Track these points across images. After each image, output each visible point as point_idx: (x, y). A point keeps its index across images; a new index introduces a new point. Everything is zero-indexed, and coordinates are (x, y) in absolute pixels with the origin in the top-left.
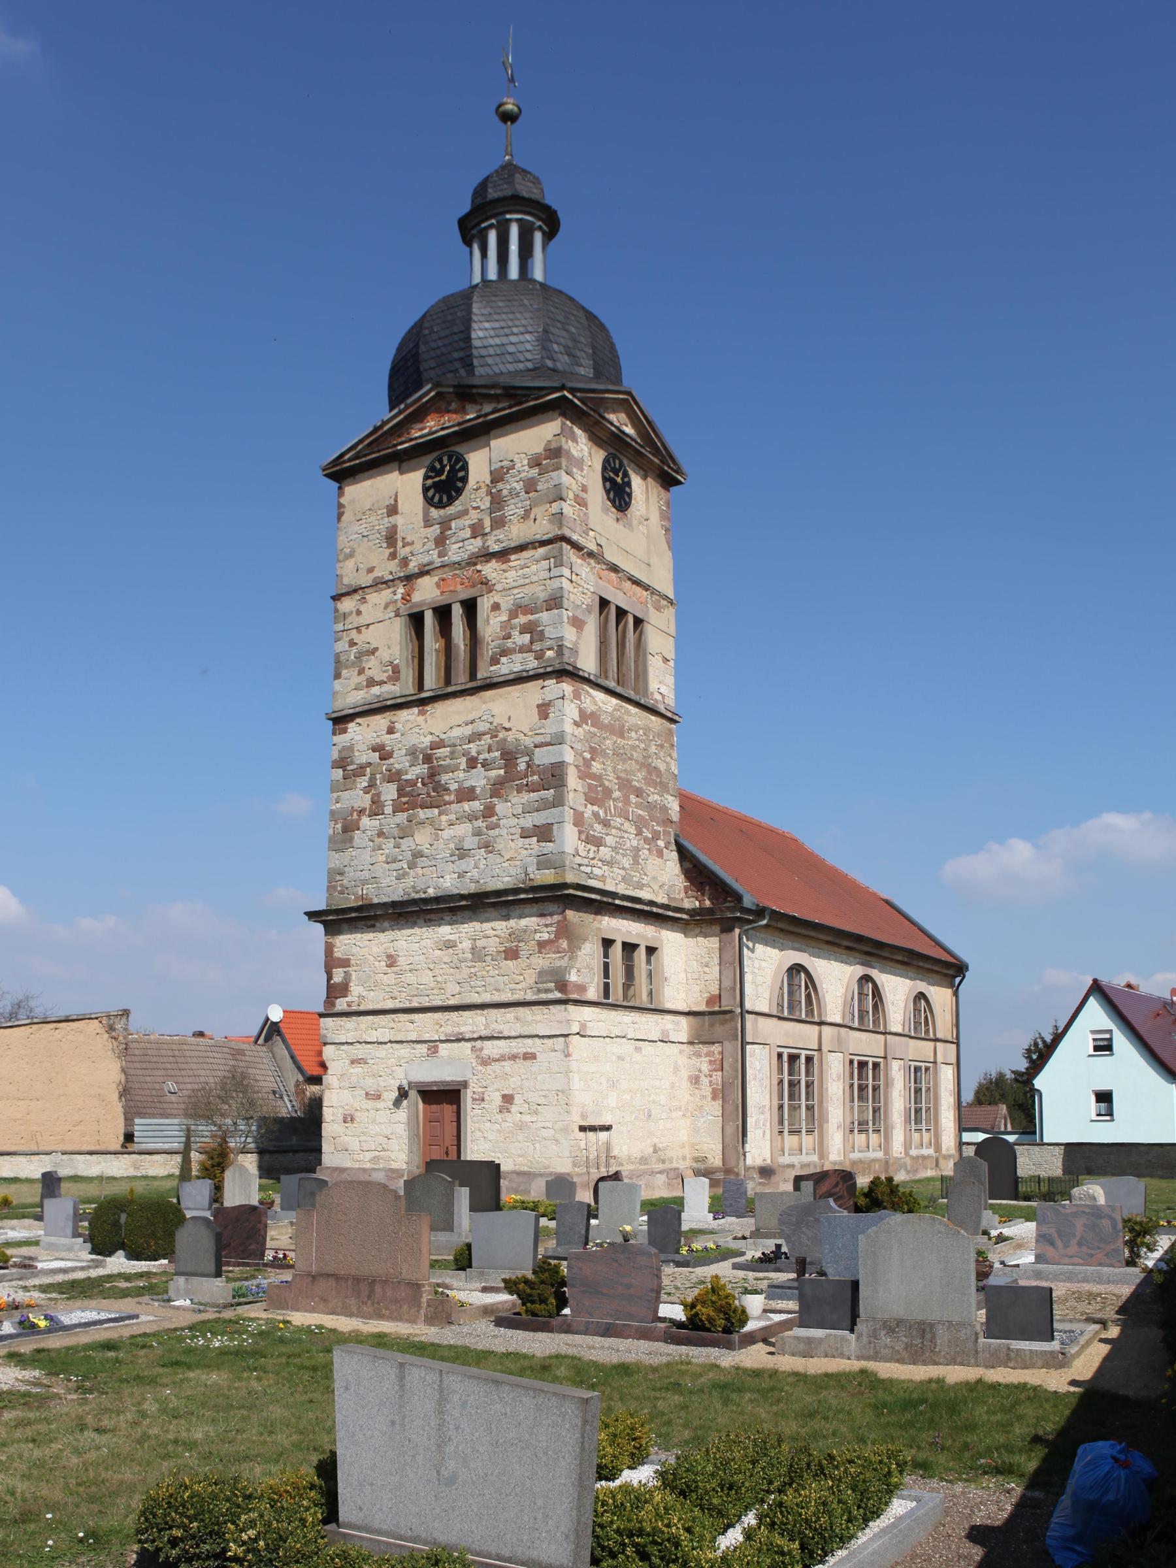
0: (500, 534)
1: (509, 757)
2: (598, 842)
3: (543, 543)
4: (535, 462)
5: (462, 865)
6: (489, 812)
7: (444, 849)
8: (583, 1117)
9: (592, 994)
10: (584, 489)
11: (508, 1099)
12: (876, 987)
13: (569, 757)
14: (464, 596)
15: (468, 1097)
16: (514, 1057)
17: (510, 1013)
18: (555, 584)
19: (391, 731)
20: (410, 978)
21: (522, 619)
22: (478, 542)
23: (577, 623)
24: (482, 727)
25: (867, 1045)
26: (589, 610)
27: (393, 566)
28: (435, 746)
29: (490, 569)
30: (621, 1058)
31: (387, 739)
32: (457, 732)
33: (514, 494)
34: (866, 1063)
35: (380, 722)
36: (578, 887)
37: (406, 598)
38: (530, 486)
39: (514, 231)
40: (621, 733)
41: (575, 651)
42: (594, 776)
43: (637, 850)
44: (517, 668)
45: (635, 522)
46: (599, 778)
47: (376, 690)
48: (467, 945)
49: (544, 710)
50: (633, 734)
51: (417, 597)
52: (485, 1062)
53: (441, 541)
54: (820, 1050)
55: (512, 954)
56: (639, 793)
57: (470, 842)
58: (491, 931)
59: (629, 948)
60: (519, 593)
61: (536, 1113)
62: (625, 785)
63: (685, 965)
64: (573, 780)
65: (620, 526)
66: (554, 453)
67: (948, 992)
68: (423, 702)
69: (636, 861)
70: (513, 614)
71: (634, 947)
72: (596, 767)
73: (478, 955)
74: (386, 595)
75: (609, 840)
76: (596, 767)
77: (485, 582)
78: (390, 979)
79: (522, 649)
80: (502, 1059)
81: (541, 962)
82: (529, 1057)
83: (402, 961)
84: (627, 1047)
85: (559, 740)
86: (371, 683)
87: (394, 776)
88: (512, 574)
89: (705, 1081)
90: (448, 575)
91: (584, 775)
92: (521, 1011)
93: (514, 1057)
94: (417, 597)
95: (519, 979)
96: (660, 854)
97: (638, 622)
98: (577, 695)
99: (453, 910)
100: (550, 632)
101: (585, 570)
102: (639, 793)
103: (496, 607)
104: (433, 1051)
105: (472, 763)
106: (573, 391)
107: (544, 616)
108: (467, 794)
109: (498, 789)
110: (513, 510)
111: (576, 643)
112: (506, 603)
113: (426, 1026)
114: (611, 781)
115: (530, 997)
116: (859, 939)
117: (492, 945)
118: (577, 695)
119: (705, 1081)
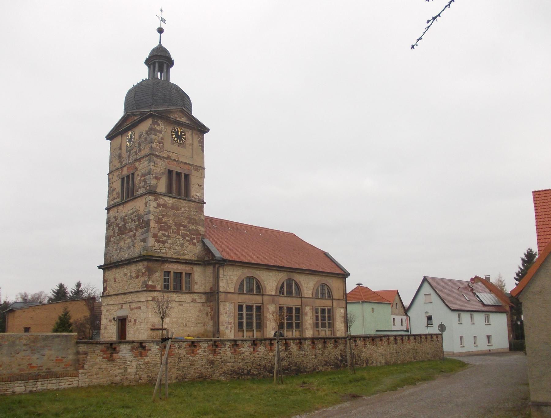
1: (139, 217)
2: (164, 242)
3: (147, 156)
5: (129, 251)
6: (135, 235)
8: (153, 326)
11: (135, 321)
12: (297, 284)
13: (151, 217)
18: (149, 167)
19: (117, 212)
21: (143, 178)
23: (157, 178)
24: (134, 210)
27: (119, 164)
28: (126, 216)
29: (137, 164)
31: (117, 215)
32: (130, 212)
33: (143, 142)
38: (146, 139)
39: (157, 65)
40: (177, 209)
42: (163, 223)
45: (187, 146)
47: (115, 201)
48: (129, 275)
49: (146, 204)
50: (183, 209)
51: (123, 174)
52: (131, 309)
53: (129, 156)
54: (263, 304)
55: (137, 277)
56: (184, 226)
60: (143, 171)
61: (140, 325)
63: (201, 278)
64: (152, 224)
65: (180, 148)
66: (151, 131)
68: (124, 203)
72: (164, 220)
82: (140, 308)
83: (117, 280)
85: (149, 213)
89: (209, 314)
90: (129, 166)
91: (157, 222)
95: (137, 284)
96: (194, 244)
97: (187, 176)
103: (138, 175)
106: (153, 111)
107: (147, 177)
108: (131, 230)
113: (120, 300)
114: (171, 223)
115: (140, 289)
116: (279, 267)
117: (134, 274)
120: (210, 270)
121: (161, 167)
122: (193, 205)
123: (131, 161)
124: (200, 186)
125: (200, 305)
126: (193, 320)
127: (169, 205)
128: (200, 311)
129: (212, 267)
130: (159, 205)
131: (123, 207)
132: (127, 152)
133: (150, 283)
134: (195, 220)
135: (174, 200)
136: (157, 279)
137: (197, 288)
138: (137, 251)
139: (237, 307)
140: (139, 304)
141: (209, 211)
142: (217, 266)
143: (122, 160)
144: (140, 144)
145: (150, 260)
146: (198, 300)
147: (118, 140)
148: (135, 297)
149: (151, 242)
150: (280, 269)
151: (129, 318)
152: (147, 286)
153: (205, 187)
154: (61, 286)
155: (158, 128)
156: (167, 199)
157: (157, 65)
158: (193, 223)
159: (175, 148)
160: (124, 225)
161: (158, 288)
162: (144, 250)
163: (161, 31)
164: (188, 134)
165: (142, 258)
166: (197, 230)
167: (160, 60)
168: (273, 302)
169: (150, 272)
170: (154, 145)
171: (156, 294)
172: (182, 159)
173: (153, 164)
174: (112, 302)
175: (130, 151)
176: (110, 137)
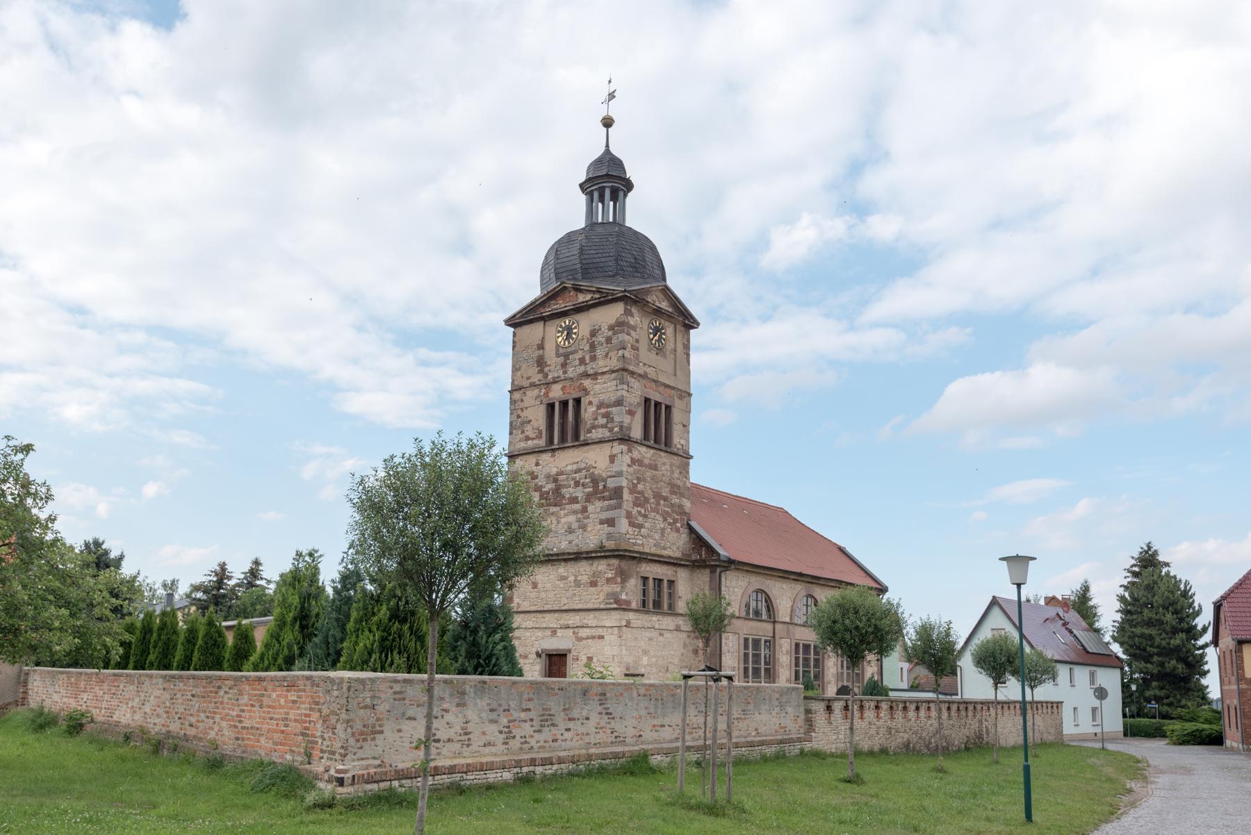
0: (593, 365)
1: (595, 481)
2: (640, 526)
3: (613, 372)
4: (611, 328)
5: (570, 537)
6: (585, 510)
7: (561, 529)
8: (628, 669)
9: (634, 605)
10: (637, 341)
14: (576, 396)
15: (569, 658)
16: (593, 637)
17: (592, 615)
19: (537, 464)
20: (543, 595)
21: (603, 411)
22: (582, 368)
23: (631, 413)
24: (583, 465)
25: (762, 629)
26: (639, 404)
29: (587, 383)
30: (651, 639)
31: (534, 468)
32: (569, 468)
34: (759, 640)
35: (532, 459)
36: (626, 550)
37: (546, 394)
38: (609, 340)
40: (655, 468)
41: (629, 428)
42: (639, 492)
43: (663, 530)
44: (600, 436)
46: (642, 493)
47: (530, 442)
48: (572, 578)
49: (612, 459)
51: (551, 395)
52: (579, 639)
53: (564, 365)
55: (593, 584)
56: (665, 499)
57: (575, 525)
58: (584, 570)
59: (659, 581)
60: (602, 397)
62: (658, 496)
64: (626, 495)
65: (659, 357)
66: (618, 327)
67: (515, 616)
69: (663, 535)
70: (599, 407)
71: (660, 581)
72: (640, 487)
73: (578, 584)
74: (536, 392)
75: (647, 525)
76: (640, 487)
77: (585, 390)
78: (533, 595)
79: (602, 426)
80: (588, 638)
81: (608, 589)
82: (601, 637)
84: (654, 634)
86: (527, 438)
87: (538, 489)
88: (597, 387)
89: (701, 652)
90: (567, 383)
91: (632, 491)
92: (597, 613)
93: (593, 637)
94: (551, 395)
95: (596, 597)
96: (678, 531)
97: (668, 408)
98: (630, 451)
99: (566, 560)
100: (617, 419)
101: (636, 384)
102: (665, 499)
103: (590, 403)
104: (554, 632)
105: (577, 484)
107: (614, 410)
108: (574, 500)
109: (589, 498)
110: (600, 352)
111: (630, 424)
112: (595, 401)
113: (550, 620)
114: (648, 494)
115: (602, 606)
116: (801, 574)
117: (584, 579)
118: (630, 451)
119: (701, 652)
120: (704, 577)
121: (635, 393)
122: (676, 460)
123: (570, 374)
124: (684, 426)
125: (684, 635)
126: (676, 661)
127: (647, 462)
128: (685, 646)
129: (708, 571)
130: (633, 461)
131: (553, 456)
132: (558, 355)
133: (624, 597)
134: (679, 487)
135: (652, 451)
136: (631, 591)
137: (681, 607)
138: (593, 537)
139: (742, 642)
140: (600, 632)
141: (699, 474)
142: (718, 570)
143: (546, 369)
144: (593, 347)
145: (624, 556)
146: (683, 628)
147: (534, 332)
148: (590, 619)
149: (623, 526)
150: (798, 577)
151: (574, 653)
152: (617, 601)
153: (692, 427)
154: (223, 566)
155: (632, 321)
156: (643, 449)
157: (608, 193)
158: (675, 493)
159: (653, 355)
160: (557, 491)
161: (634, 605)
162: (608, 539)
163: (608, 123)
164: (669, 330)
165: (600, 554)
166: (681, 506)
167: (608, 181)
168: (788, 635)
169: (623, 576)
170: (627, 354)
171: (631, 615)
172: (662, 379)
173: (625, 387)
174: (529, 624)
175: (566, 356)
176: (515, 322)
